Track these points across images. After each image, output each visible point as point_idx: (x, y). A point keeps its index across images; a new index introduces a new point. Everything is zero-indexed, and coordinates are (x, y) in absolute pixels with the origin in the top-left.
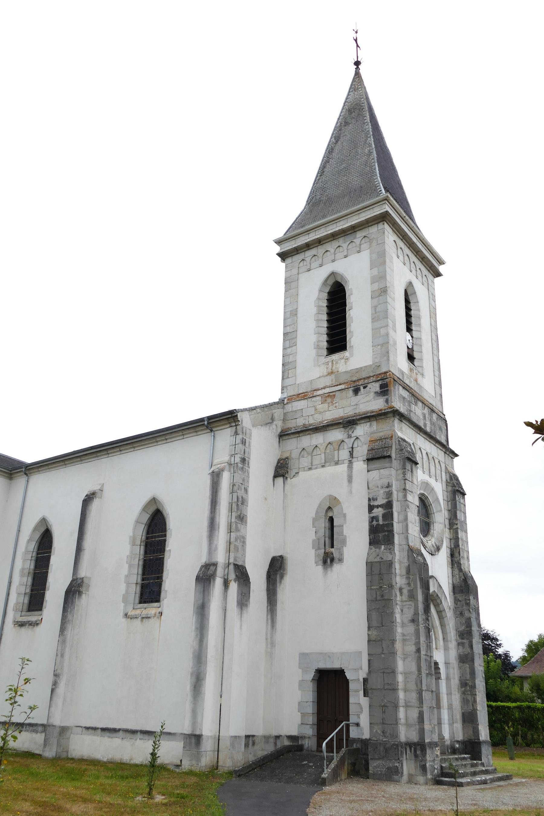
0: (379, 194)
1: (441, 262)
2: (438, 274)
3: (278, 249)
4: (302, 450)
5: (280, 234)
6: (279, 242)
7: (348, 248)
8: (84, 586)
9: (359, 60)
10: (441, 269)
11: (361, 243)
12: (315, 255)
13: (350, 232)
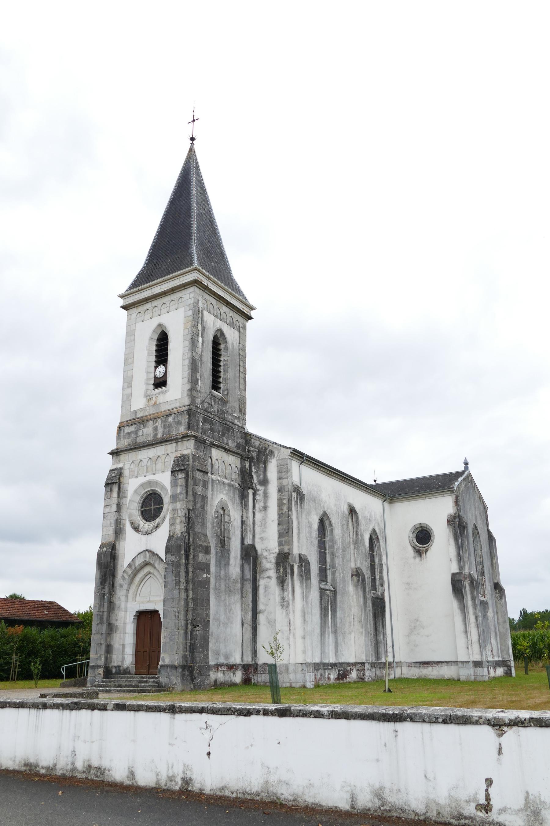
0: (191, 264)
1: (252, 308)
2: (250, 318)
3: (121, 302)
4: (140, 462)
5: (123, 290)
6: (122, 297)
7: (162, 308)
8: (240, 504)
9: (194, 137)
10: (253, 314)
11: (162, 308)
12: (173, 300)
13: (164, 296)
